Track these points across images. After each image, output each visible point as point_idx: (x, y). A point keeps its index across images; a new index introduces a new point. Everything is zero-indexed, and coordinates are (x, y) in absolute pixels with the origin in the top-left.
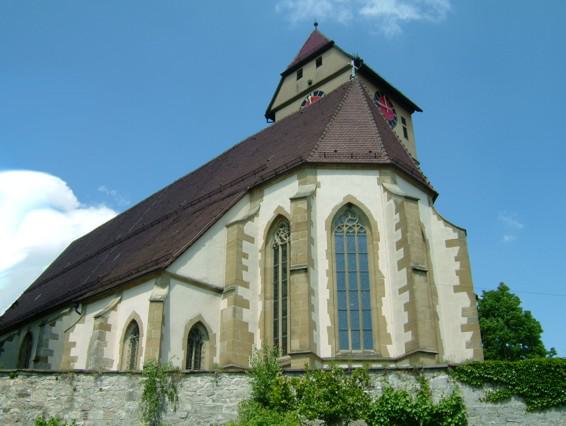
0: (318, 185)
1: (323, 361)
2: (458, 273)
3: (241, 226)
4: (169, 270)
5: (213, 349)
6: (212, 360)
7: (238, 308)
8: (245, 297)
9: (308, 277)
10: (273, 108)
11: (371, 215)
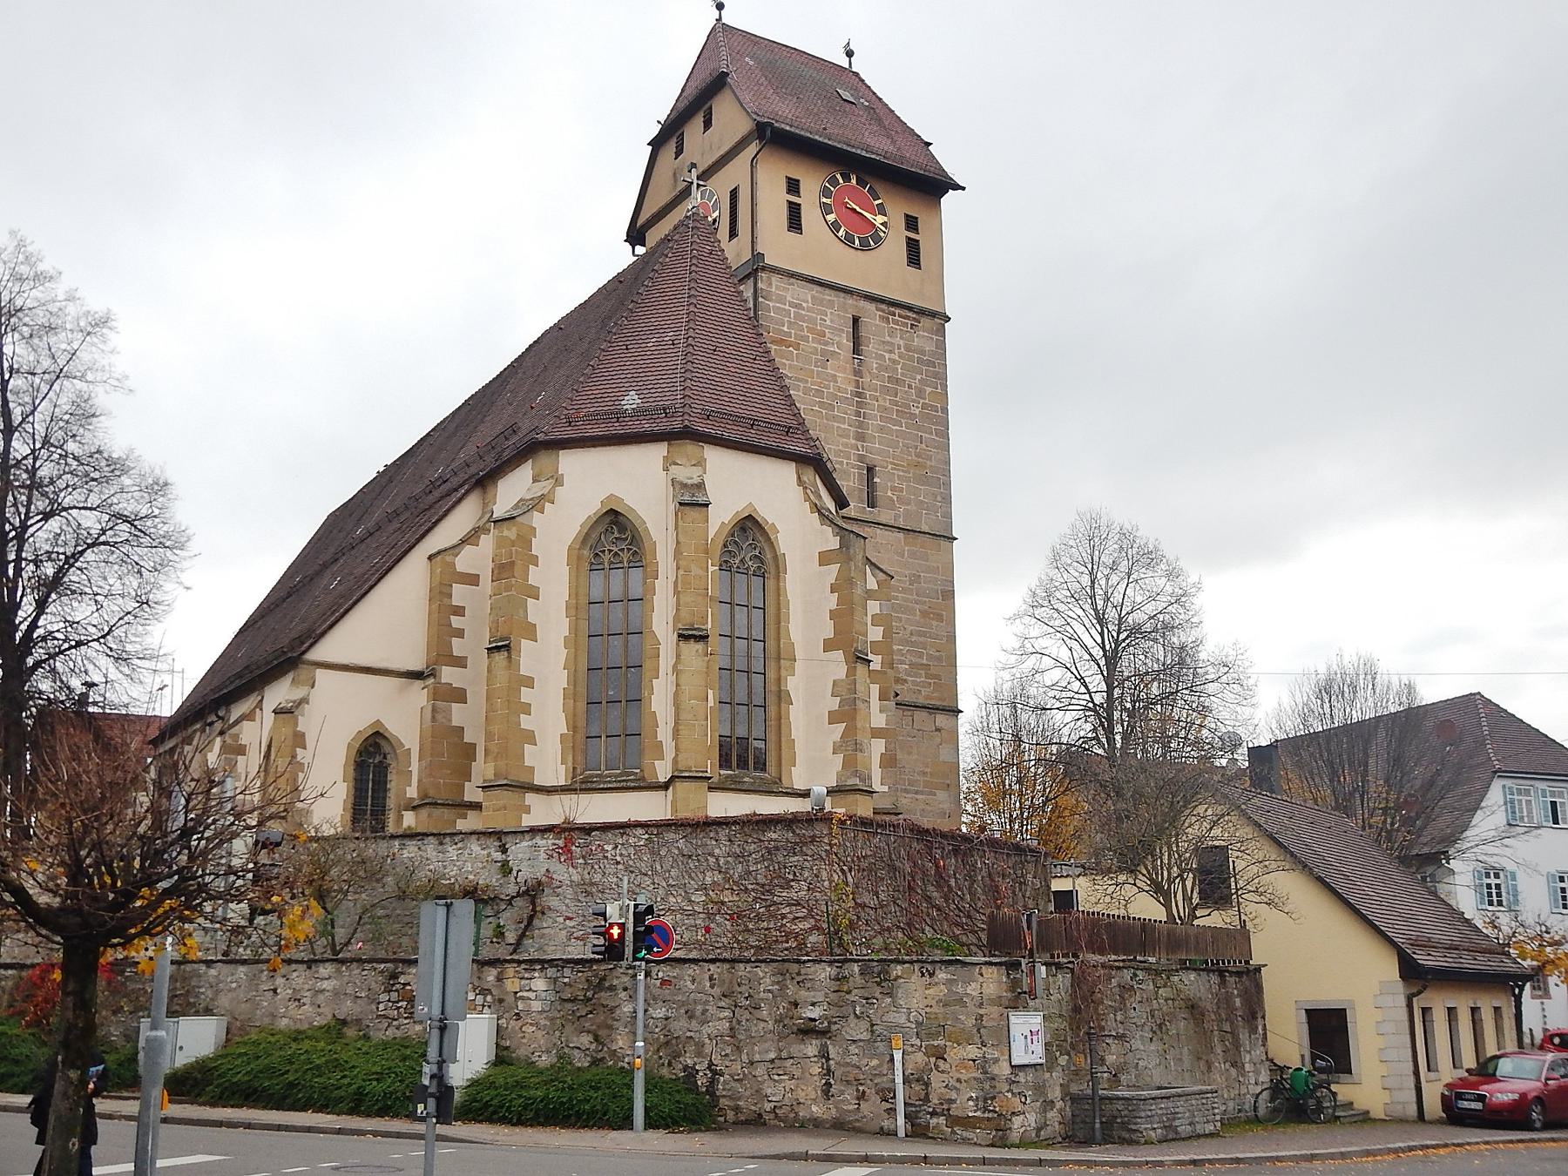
2: (833, 615)
3: (448, 559)
9: (509, 657)
10: (639, 224)
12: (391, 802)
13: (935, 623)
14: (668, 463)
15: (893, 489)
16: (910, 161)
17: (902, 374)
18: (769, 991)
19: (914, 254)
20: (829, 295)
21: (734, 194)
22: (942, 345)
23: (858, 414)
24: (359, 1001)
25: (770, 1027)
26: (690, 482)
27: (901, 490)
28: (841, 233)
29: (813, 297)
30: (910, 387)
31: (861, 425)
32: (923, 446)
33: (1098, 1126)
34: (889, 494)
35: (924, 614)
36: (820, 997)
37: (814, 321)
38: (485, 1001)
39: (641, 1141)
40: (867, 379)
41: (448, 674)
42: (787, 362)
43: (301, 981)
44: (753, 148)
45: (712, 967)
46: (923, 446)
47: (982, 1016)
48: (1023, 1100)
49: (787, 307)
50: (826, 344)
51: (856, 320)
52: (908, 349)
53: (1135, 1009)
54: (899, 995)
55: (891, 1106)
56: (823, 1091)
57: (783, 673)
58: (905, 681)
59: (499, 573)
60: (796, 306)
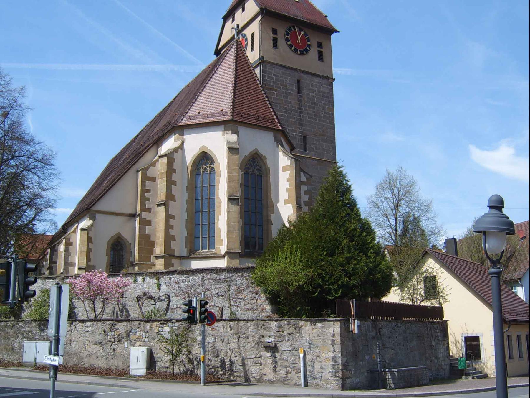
15: (313, 144)
16: (319, 22)
18: (253, 331)
19: (321, 57)
20: (288, 72)
21: (253, 35)
22: (332, 90)
23: (300, 116)
24: (101, 335)
25: (253, 345)
28: (293, 48)
29: (282, 73)
30: (320, 106)
31: (301, 120)
33: (380, 382)
34: (312, 146)
36: (272, 334)
38: (146, 336)
39: (201, 389)
40: (303, 103)
42: (273, 97)
44: (260, 18)
45: (231, 323)
47: (334, 340)
48: (351, 372)
49: (272, 76)
50: (287, 89)
51: (299, 81)
53: (397, 337)
54: (303, 333)
55: (299, 375)
56: (273, 370)
57: (269, 213)
59: (161, 176)
60: (275, 76)
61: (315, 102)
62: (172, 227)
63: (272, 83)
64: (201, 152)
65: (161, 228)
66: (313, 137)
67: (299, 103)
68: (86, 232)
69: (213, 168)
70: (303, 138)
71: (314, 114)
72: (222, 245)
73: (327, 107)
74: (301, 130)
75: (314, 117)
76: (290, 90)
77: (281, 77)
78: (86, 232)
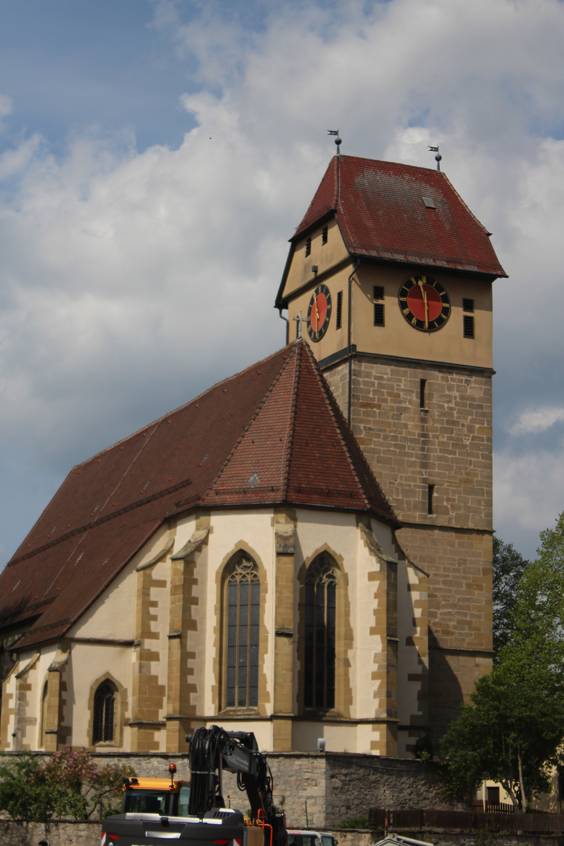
0: (209, 531)
1: (548, 600)
4: (69, 635)
5: (125, 704)
6: (123, 715)
7: (143, 662)
8: (153, 650)
10: (285, 294)
11: (261, 563)
12: (117, 720)
13: (477, 592)
14: (274, 522)
15: (448, 500)
17: (458, 417)
23: (423, 449)
26: (285, 535)
27: (454, 500)
28: (414, 321)
29: (392, 370)
30: (463, 425)
31: (425, 457)
32: (472, 467)
35: (469, 586)
37: (391, 387)
40: (430, 424)
41: (149, 644)
43: (71, 831)
44: (350, 269)
46: (472, 467)
49: (372, 380)
50: (400, 402)
52: (462, 398)
58: (454, 633)
61: (455, 419)
62: (191, 672)
63: (372, 393)
64: (237, 550)
65: (175, 674)
66: (448, 486)
67: (423, 424)
68: (57, 674)
69: (255, 576)
70: (427, 490)
71: (451, 442)
72: (268, 701)
73: (477, 426)
74: (424, 477)
75: (451, 448)
76: (405, 402)
77: (388, 380)
78: (57, 674)
